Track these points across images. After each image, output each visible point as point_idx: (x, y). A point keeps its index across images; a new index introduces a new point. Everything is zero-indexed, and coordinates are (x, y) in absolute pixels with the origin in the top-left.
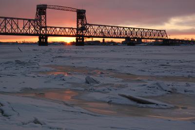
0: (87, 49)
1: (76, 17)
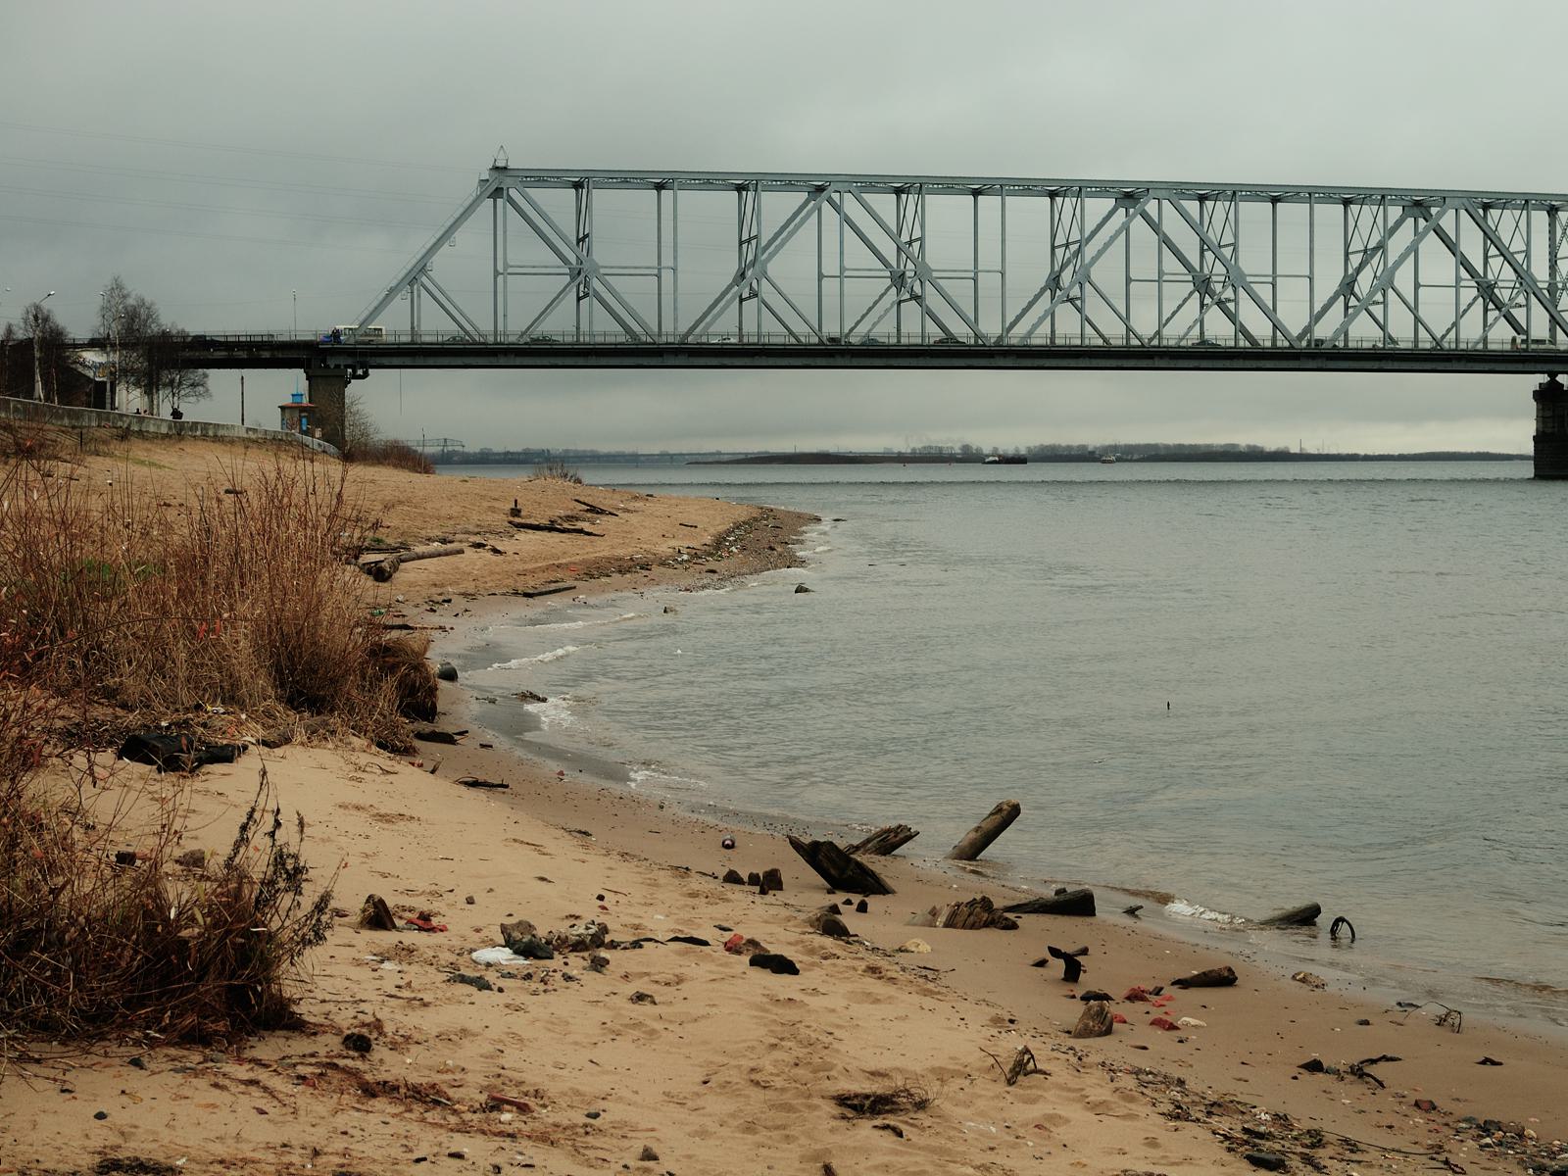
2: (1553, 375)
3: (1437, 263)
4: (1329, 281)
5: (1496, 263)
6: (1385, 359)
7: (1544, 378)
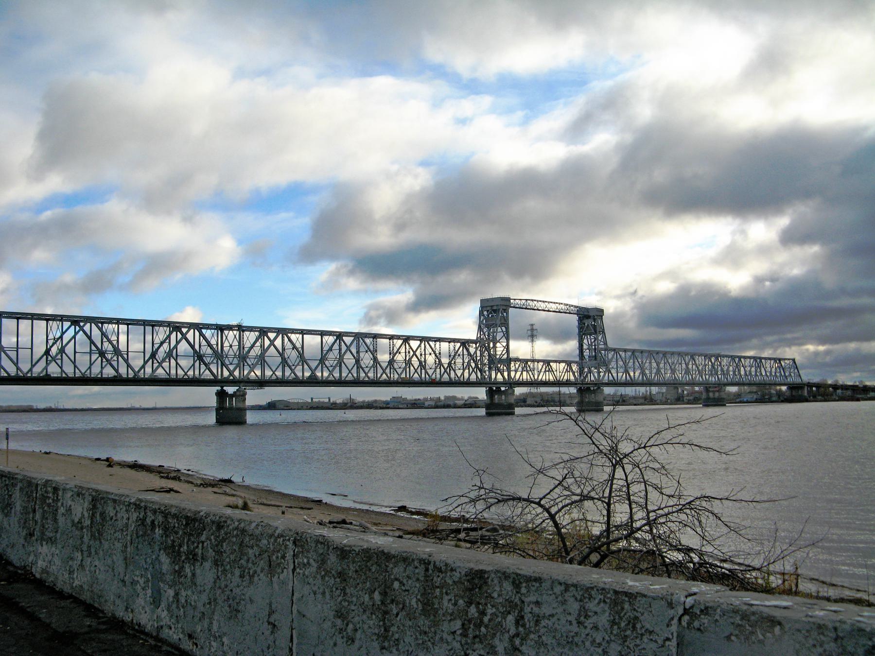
2: (222, 387)
4: (40, 350)
5: (106, 344)
7: (219, 388)
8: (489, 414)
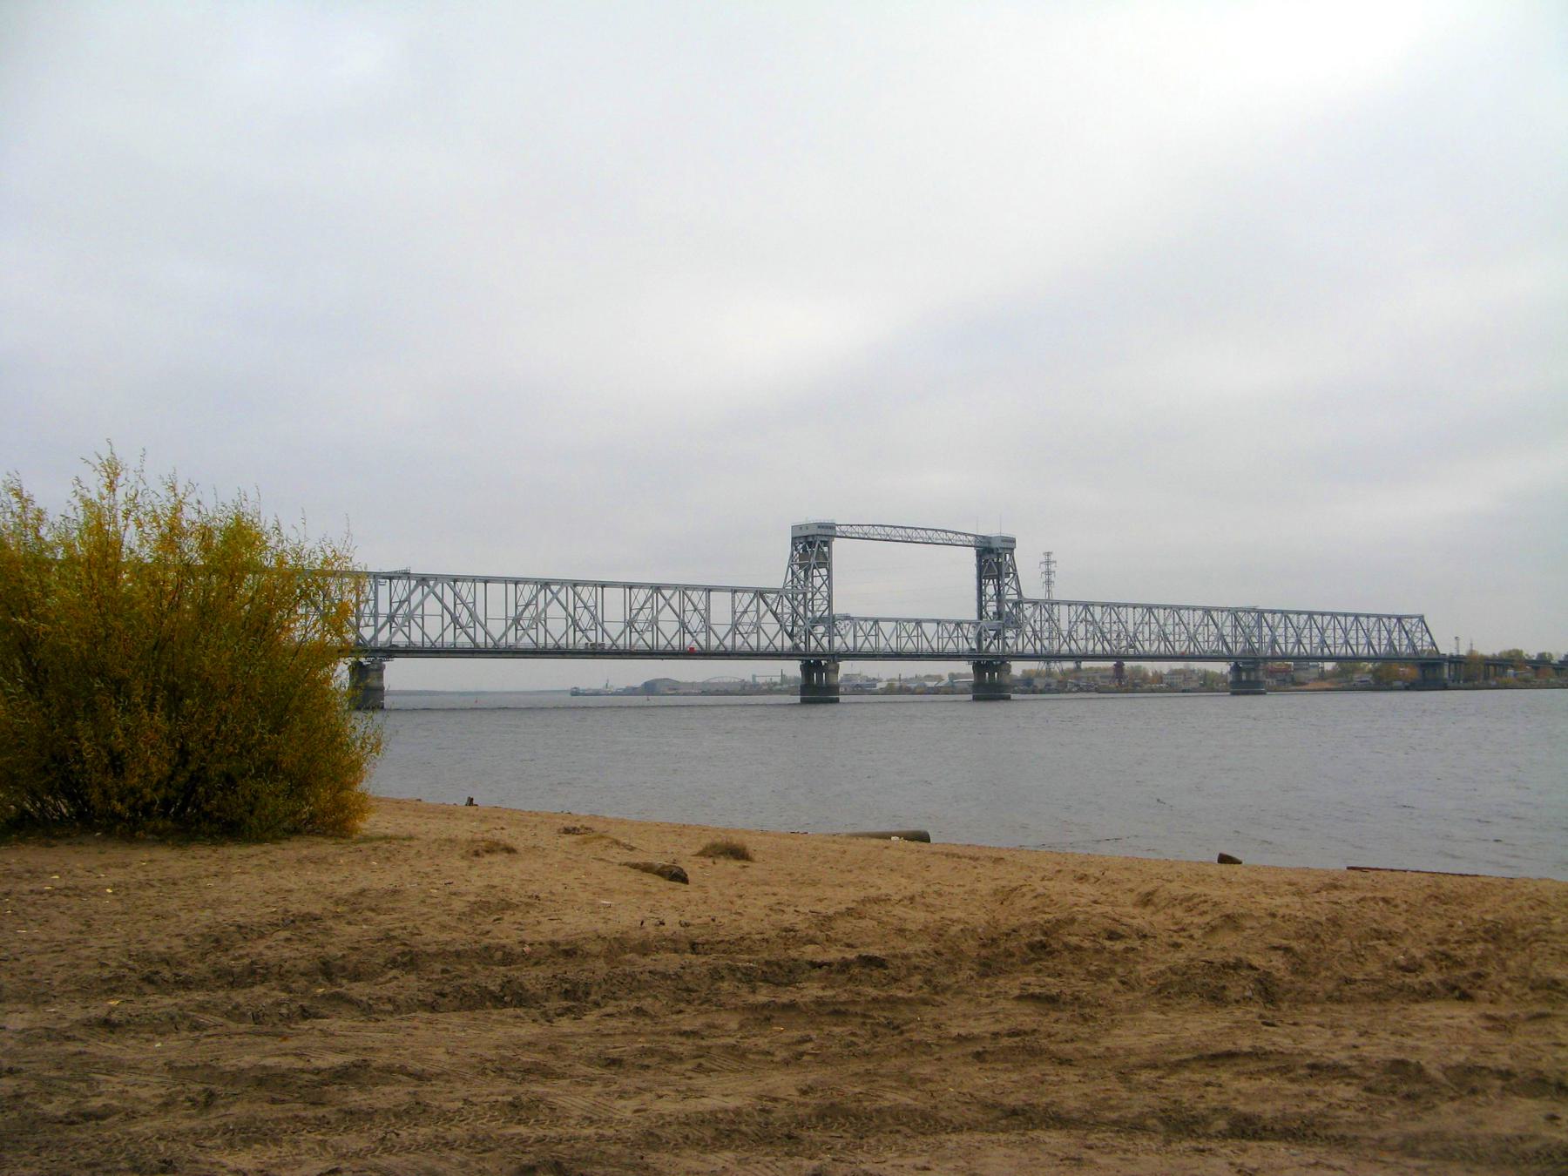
0: (1020, 709)
1: (974, 571)
2: (1079, 667)
3: (432, 605)
5: (460, 607)
6: (475, 652)
8: (804, 702)
